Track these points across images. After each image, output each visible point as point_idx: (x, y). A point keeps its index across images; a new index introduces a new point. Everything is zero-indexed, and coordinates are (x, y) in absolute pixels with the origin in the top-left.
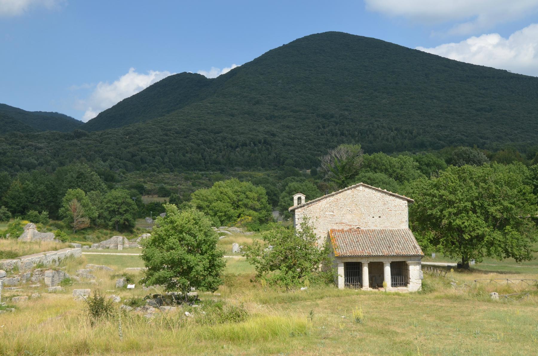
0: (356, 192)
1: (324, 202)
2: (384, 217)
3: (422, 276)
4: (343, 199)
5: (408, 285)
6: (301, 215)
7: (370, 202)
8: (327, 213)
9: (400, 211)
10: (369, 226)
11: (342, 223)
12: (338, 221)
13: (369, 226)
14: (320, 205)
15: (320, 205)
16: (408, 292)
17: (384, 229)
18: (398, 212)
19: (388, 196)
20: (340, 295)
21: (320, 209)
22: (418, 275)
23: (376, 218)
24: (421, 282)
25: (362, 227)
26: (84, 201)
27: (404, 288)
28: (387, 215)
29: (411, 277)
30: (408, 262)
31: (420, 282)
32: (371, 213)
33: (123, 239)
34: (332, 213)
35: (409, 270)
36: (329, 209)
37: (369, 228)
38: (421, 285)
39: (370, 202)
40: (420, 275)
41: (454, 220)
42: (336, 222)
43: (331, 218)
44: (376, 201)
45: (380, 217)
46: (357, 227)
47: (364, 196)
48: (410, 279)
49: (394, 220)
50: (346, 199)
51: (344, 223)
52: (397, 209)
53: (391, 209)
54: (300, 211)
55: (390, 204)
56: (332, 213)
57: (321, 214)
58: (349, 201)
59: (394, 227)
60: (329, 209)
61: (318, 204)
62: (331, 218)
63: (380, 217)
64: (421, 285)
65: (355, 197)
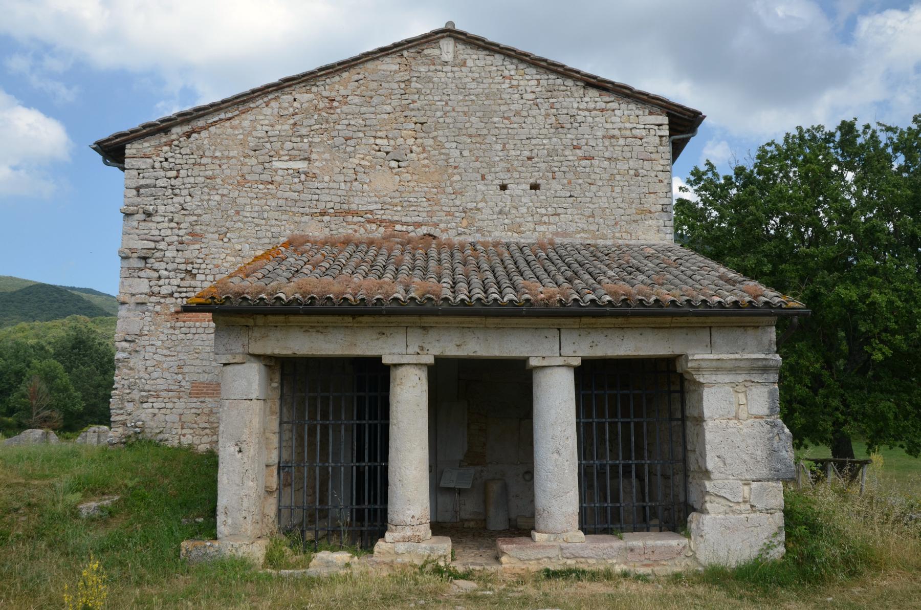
0: (423, 69)
1: (267, 111)
2: (556, 186)
3: (788, 454)
4: (357, 100)
5: (693, 516)
6: (151, 173)
7: (486, 117)
8: (277, 165)
9: (632, 163)
10: (479, 230)
11: (349, 212)
12: (328, 200)
13: (479, 230)
14: (246, 124)
15: (246, 124)
16: (693, 566)
17: (558, 240)
18: (622, 166)
19: (578, 91)
20: (629, 551)
21: (243, 144)
22: (760, 453)
23: (518, 189)
24: (778, 501)
25: (446, 230)
26: (59, 381)
27: (674, 542)
28: (570, 176)
29: (711, 463)
30: (689, 352)
31: (775, 496)
32: (491, 165)
33: (46, 435)
34: (302, 165)
35: (700, 420)
36: (288, 145)
37: (478, 237)
38: (779, 518)
39: (486, 117)
40: (773, 452)
41: (830, 287)
42: (321, 206)
43: (299, 187)
44: (518, 113)
45: (535, 187)
46: (424, 230)
47: (462, 88)
48: (706, 474)
49: (603, 202)
50: (375, 100)
51: (356, 213)
52: (617, 153)
53: (593, 153)
54: (148, 151)
55: (585, 129)
56: (302, 165)
57: (246, 169)
58: (389, 108)
59: (604, 237)
60: (288, 145)
61: (235, 122)
62: (299, 187)
63: (535, 187)
64: (779, 518)
65: (419, 92)
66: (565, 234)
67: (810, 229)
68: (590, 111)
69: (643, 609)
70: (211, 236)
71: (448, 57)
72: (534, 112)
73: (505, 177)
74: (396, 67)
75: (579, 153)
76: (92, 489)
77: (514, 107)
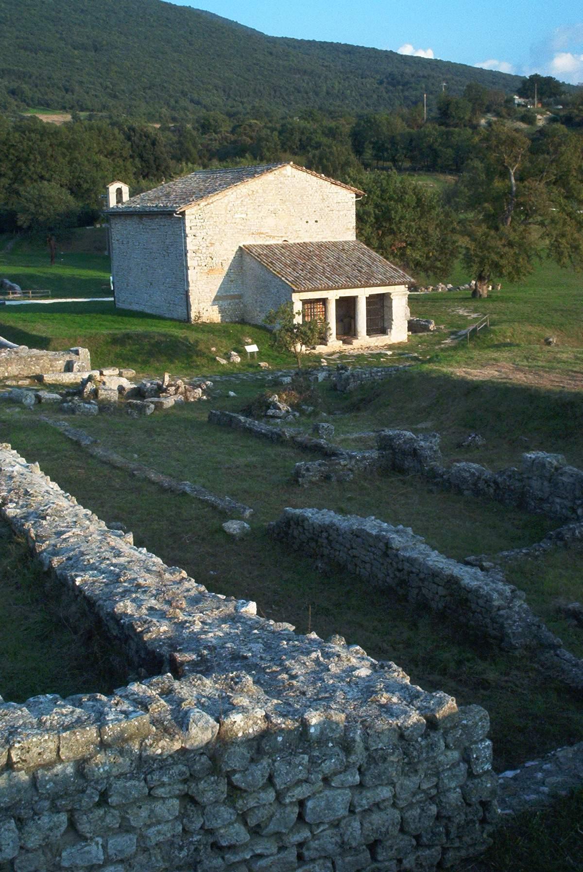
6: (195, 221)
12: (254, 229)
18: (341, 213)
23: (312, 222)
32: (303, 214)
45: (316, 221)
51: (262, 234)
54: (194, 212)
60: (240, 209)
61: (222, 201)
63: (316, 221)
66: (325, 238)
67: (298, 320)
68: (142, 521)
69: (0, 450)
70: (217, 244)
71: (289, 174)
72: (316, 194)
73: (308, 219)
74: (273, 179)
75: (329, 209)
76: (312, 539)
77: (310, 192)
